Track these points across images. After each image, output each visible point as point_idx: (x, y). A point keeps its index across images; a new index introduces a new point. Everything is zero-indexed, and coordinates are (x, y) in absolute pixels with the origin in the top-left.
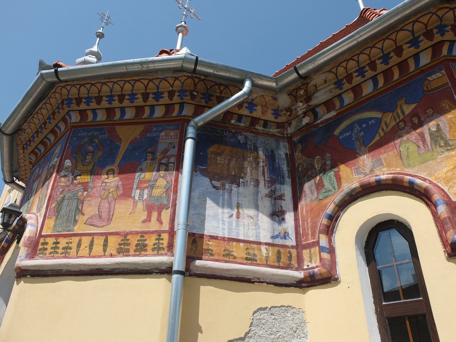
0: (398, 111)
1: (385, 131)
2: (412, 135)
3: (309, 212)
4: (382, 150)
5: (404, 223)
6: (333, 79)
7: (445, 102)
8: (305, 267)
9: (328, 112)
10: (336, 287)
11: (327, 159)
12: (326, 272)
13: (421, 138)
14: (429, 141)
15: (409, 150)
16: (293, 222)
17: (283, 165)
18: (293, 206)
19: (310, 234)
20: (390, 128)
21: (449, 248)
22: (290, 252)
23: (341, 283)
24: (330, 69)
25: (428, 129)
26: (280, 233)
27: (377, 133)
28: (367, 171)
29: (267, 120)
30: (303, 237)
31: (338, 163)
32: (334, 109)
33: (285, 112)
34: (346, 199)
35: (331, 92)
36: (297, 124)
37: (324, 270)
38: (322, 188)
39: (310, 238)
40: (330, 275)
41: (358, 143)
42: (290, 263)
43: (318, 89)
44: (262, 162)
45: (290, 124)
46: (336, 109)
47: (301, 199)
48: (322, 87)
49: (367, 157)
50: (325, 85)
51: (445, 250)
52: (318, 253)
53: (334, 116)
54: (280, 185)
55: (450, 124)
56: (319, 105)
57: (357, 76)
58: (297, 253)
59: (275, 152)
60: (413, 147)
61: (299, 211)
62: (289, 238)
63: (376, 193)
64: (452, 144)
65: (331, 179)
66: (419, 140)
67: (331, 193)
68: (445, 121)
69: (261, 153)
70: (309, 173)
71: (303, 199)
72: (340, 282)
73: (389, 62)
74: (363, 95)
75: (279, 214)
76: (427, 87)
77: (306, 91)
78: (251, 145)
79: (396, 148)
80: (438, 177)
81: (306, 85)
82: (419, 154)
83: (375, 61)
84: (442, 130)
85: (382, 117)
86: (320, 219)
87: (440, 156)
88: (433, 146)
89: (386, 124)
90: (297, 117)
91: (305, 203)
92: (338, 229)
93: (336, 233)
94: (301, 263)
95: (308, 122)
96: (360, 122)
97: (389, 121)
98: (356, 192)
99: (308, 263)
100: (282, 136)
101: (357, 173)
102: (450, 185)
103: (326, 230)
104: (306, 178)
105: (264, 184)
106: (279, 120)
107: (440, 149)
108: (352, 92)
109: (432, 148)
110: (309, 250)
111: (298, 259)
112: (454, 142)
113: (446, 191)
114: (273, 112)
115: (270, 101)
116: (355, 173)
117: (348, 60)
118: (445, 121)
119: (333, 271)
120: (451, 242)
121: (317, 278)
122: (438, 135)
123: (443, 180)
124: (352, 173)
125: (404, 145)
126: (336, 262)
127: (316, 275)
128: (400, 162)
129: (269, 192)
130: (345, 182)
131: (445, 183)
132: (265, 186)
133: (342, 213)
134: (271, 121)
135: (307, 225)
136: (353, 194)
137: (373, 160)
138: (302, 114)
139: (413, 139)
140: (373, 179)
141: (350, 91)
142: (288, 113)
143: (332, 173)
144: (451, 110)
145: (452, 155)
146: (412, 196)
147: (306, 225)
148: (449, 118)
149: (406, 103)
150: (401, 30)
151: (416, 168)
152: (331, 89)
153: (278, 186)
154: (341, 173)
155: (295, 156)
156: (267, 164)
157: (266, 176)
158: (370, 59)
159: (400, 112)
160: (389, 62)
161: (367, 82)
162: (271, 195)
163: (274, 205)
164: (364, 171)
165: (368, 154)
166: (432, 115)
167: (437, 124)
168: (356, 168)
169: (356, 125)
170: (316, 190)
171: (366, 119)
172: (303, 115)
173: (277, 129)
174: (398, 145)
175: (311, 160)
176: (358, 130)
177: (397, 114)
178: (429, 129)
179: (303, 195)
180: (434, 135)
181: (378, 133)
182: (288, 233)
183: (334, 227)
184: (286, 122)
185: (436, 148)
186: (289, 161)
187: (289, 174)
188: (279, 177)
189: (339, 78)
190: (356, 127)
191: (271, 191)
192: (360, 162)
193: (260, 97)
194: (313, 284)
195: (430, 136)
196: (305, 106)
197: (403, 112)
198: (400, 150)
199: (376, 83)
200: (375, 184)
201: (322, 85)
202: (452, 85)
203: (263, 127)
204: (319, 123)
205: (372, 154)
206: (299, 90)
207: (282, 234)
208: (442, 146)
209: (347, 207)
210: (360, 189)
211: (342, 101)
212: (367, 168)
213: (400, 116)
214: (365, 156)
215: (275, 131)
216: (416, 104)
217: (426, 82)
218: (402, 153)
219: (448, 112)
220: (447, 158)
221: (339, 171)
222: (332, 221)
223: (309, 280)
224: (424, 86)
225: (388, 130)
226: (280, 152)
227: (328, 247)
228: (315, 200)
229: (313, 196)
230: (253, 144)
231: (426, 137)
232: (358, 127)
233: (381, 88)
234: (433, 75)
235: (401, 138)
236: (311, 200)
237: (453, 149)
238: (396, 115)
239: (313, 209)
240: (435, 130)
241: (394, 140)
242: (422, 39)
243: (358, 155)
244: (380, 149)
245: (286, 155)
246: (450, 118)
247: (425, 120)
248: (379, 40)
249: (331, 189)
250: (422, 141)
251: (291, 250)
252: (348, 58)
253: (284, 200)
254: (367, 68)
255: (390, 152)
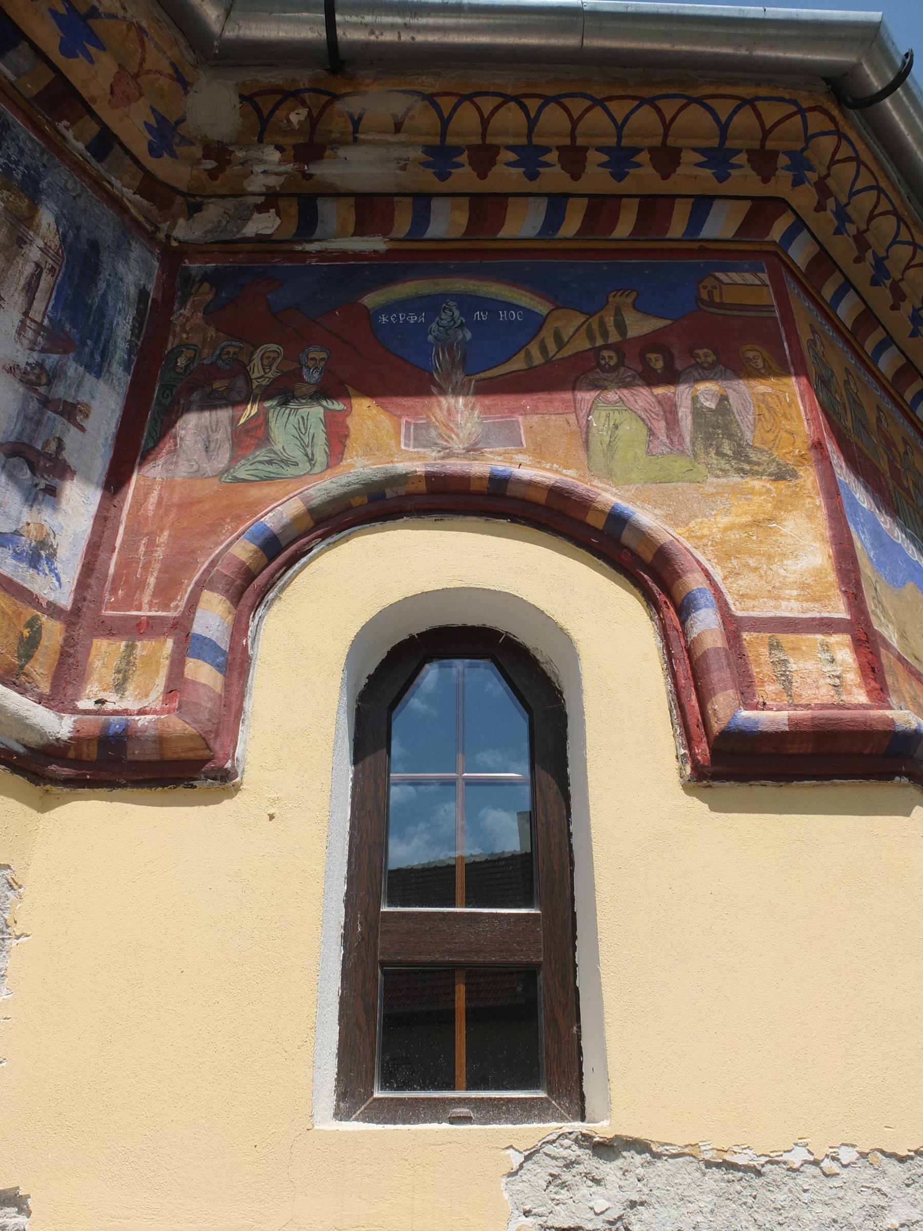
0: (606, 319)
1: (550, 355)
2: (636, 395)
3: (174, 510)
4: (526, 401)
5: (530, 648)
6: (429, 134)
7: (757, 351)
8: (85, 704)
9: (360, 231)
10: (212, 807)
11: (311, 363)
12: (191, 737)
13: (665, 412)
14: (689, 428)
15: (619, 432)
16: (90, 522)
17: (120, 314)
18: (107, 466)
19: (152, 586)
20: (570, 353)
21: (703, 750)
22: (32, 623)
23: (239, 795)
24: (434, 91)
25: (689, 397)
26: (17, 533)
27: (523, 347)
28: (458, 446)
29: (116, 138)
30: (114, 591)
31: (350, 389)
32: (384, 229)
33: (198, 151)
34: (357, 501)
35: (404, 168)
36: (224, 223)
37: (177, 725)
38: (258, 446)
39: (146, 598)
40: (201, 753)
41: (443, 355)
42: (22, 667)
43: (361, 136)
44: (41, 249)
45: (194, 209)
46: (394, 235)
47: (150, 458)
48: (378, 137)
49: (465, 405)
50: (391, 138)
51: (687, 752)
52: (167, 662)
53: (375, 251)
54: (81, 369)
55: (759, 406)
56: (337, 195)
57: (509, 164)
58: (65, 640)
59: (105, 257)
60: (630, 428)
61: (127, 493)
62: (50, 571)
63: (475, 518)
64: (755, 459)
65: (306, 429)
66: (657, 414)
67: (291, 471)
68: (748, 395)
69: (46, 218)
70: (217, 385)
71: (161, 462)
72: (237, 789)
73: (627, 173)
74: (502, 234)
75: (42, 463)
76: (710, 294)
77: (313, 121)
78: (17, 163)
79: (575, 412)
80: (698, 534)
81: (326, 98)
82: (649, 453)
83: (585, 149)
84: (734, 413)
85: (547, 315)
86: (218, 544)
87: (715, 480)
88: (700, 445)
89: (558, 337)
90: (235, 196)
91: (164, 475)
92: (284, 595)
93: (274, 608)
94: (69, 683)
95: (269, 232)
96: (468, 303)
97: (571, 333)
98: (402, 491)
99: (105, 690)
100: (150, 228)
101: (415, 439)
102: (730, 565)
103: (238, 582)
104: (195, 396)
105: (17, 323)
106: (163, 168)
107: (717, 460)
108: (467, 208)
109: (693, 450)
110: (124, 643)
111: (61, 664)
112: (764, 458)
113: (715, 579)
114: (152, 121)
115: (160, 73)
116: (407, 437)
117: (507, 98)
118: (748, 395)
119: (218, 742)
120: (722, 726)
121: (136, 752)
122: (718, 423)
123: (713, 546)
124: (398, 433)
125: (604, 414)
126: (240, 710)
127: (138, 738)
128: (582, 453)
129: (27, 364)
130: (360, 452)
131: (716, 557)
132: (19, 333)
133: (322, 545)
134: (127, 152)
135: (149, 552)
136: (389, 493)
137: (486, 419)
138: (259, 195)
139: (637, 407)
140: (479, 468)
141: (465, 201)
142: (210, 164)
143: (315, 412)
144: (770, 374)
145: (753, 488)
146: (601, 562)
147: (142, 549)
148: (760, 392)
149: (635, 306)
150: (700, 101)
151: (633, 488)
152: (408, 159)
153: (73, 369)
154: (351, 422)
155: (175, 316)
156: (57, 268)
157: (39, 305)
158: (573, 136)
159: (612, 323)
160: (627, 173)
161: (531, 199)
162: (32, 377)
163: (34, 422)
164: (446, 441)
165: (471, 399)
166: (712, 366)
167: (721, 395)
168: (416, 425)
169: (451, 303)
170: (227, 445)
171: (490, 299)
172: (262, 199)
173: (138, 196)
174: (585, 408)
175: (241, 348)
176: (453, 319)
177: (602, 324)
178: (695, 399)
179: (168, 444)
180: (706, 417)
181: (524, 350)
182: (55, 550)
183: (273, 585)
184: (182, 194)
185: (707, 453)
186: (144, 317)
187: (129, 357)
188: (89, 342)
189: (451, 140)
190: (450, 310)
191: (40, 365)
192: (437, 410)
193: (129, 29)
194: (104, 775)
195: (693, 418)
196: (289, 167)
197: (621, 327)
198: (588, 421)
199: (554, 219)
200: (484, 486)
201: (381, 132)
202: (781, 315)
203: (88, 148)
204: (308, 252)
205: (487, 401)
206: (289, 103)
207: (25, 543)
208: (726, 455)
209: (347, 532)
210: (422, 487)
211: (421, 220)
212: (458, 435)
213: (610, 334)
214: (461, 400)
215: (128, 193)
216: (669, 322)
217: (709, 282)
218: (593, 431)
219: (760, 378)
220: (735, 491)
221: (347, 413)
222: (271, 559)
223: (92, 753)
224: (701, 288)
225: (559, 356)
226: (121, 268)
227: (223, 647)
228: (216, 476)
229: (209, 461)
230: (26, 167)
231: (680, 414)
232: (457, 313)
233: (565, 239)
234: (734, 274)
235: (598, 392)
236: (198, 471)
237: (757, 473)
238: (595, 327)
239: (192, 504)
240: (713, 406)
241: (574, 389)
242: (740, 163)
243: (434, 389)
244: (521, 396)
245: (143, 294)
246: (763, 394)
247: (687, 371)
248: (629, 92)
249: (295, 460)
250: (667, 423)
251: (44, 618)
252: (509, 92)
253: (82, 429)
254: (552, 157)
255: (553, 417)
